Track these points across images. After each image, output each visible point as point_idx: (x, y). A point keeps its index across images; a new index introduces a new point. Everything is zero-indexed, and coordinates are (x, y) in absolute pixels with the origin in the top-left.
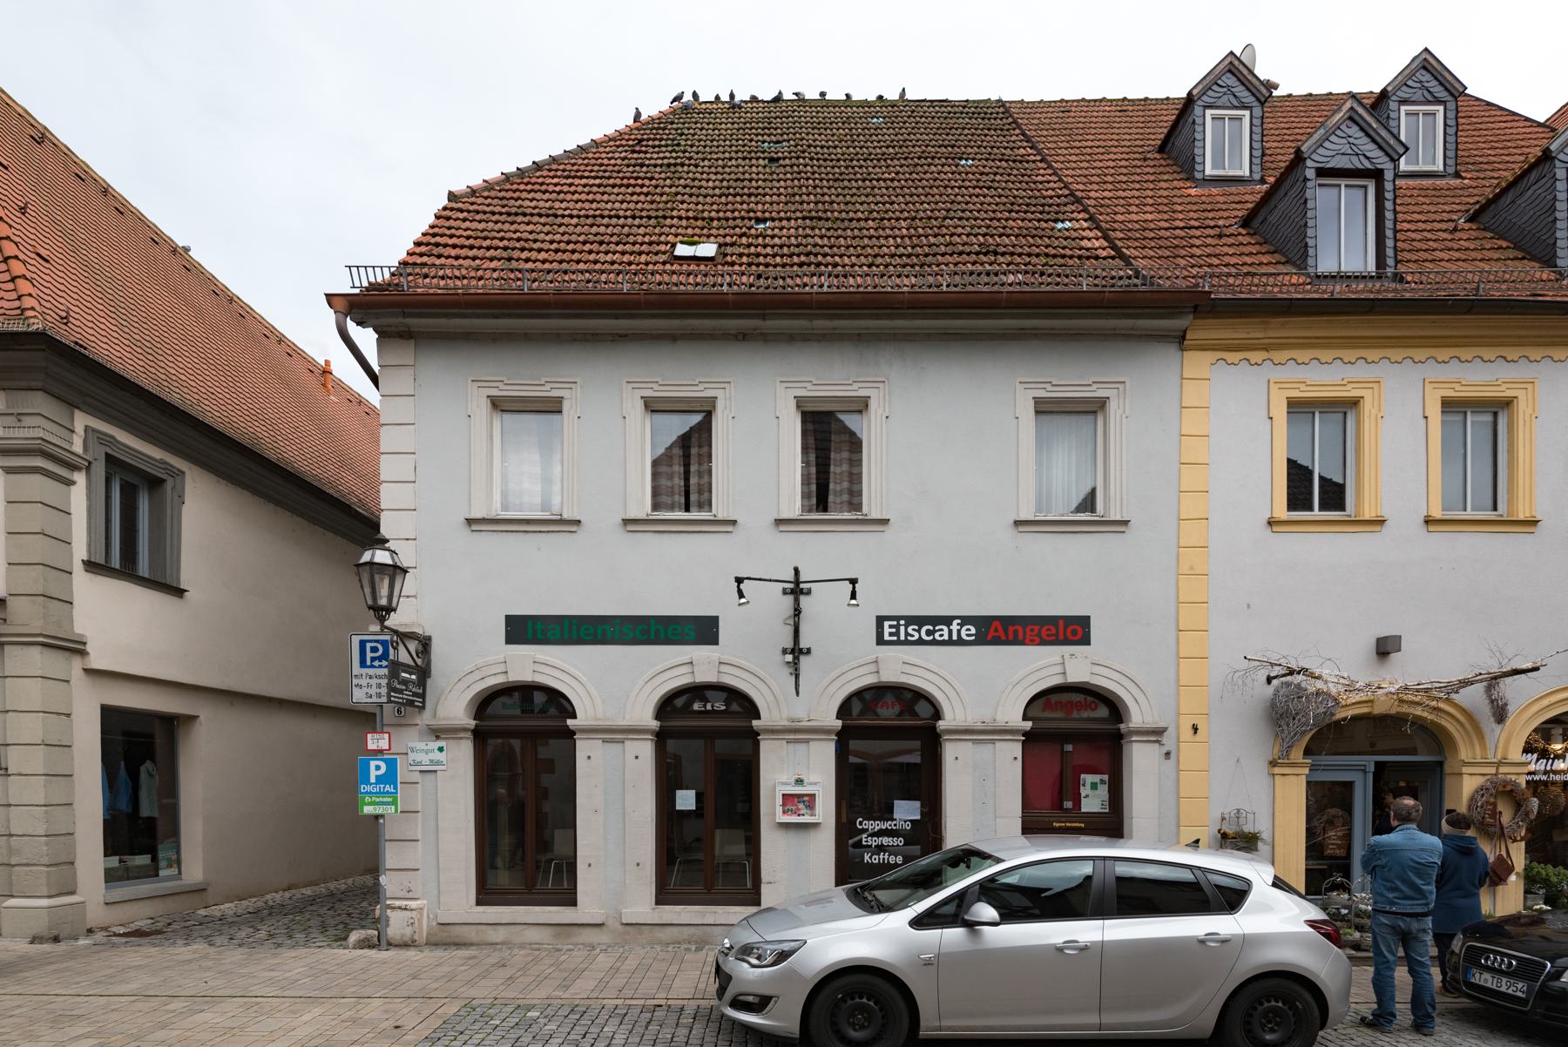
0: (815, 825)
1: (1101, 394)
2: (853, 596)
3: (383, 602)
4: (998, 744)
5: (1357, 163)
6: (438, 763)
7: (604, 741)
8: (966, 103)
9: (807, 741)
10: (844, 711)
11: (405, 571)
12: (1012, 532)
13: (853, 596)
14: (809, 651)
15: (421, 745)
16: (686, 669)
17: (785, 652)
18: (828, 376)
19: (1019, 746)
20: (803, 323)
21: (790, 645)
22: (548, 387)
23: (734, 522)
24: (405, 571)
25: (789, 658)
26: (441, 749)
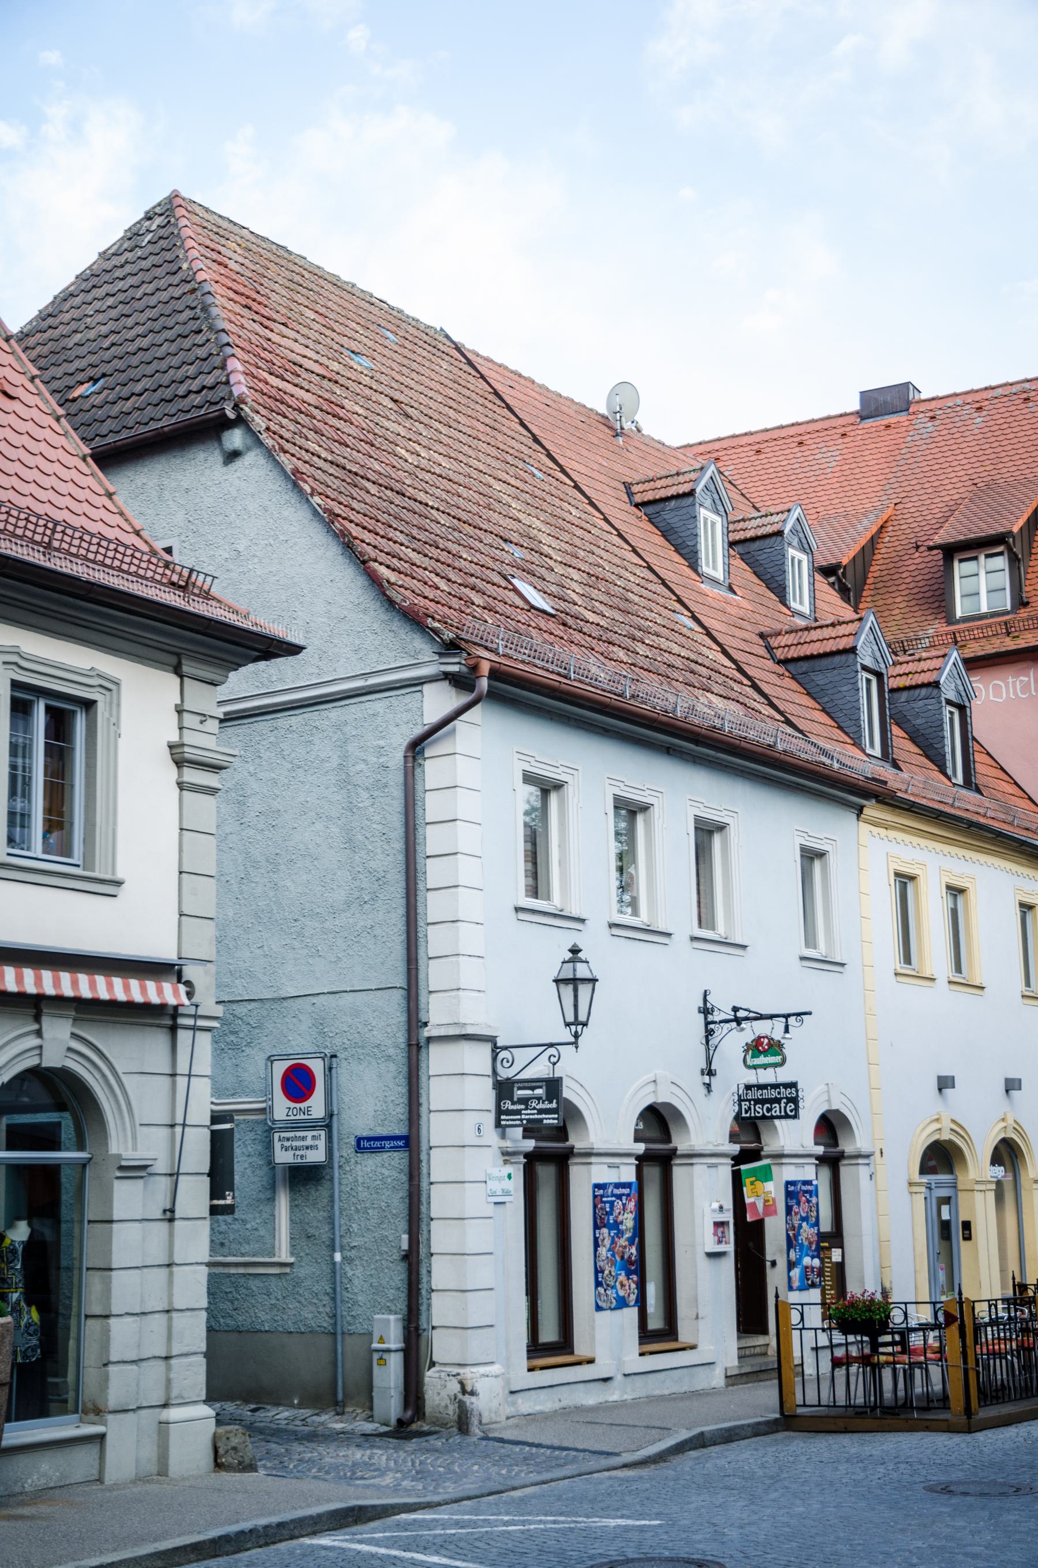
4: (806, 1167)
17: (703, 1073)
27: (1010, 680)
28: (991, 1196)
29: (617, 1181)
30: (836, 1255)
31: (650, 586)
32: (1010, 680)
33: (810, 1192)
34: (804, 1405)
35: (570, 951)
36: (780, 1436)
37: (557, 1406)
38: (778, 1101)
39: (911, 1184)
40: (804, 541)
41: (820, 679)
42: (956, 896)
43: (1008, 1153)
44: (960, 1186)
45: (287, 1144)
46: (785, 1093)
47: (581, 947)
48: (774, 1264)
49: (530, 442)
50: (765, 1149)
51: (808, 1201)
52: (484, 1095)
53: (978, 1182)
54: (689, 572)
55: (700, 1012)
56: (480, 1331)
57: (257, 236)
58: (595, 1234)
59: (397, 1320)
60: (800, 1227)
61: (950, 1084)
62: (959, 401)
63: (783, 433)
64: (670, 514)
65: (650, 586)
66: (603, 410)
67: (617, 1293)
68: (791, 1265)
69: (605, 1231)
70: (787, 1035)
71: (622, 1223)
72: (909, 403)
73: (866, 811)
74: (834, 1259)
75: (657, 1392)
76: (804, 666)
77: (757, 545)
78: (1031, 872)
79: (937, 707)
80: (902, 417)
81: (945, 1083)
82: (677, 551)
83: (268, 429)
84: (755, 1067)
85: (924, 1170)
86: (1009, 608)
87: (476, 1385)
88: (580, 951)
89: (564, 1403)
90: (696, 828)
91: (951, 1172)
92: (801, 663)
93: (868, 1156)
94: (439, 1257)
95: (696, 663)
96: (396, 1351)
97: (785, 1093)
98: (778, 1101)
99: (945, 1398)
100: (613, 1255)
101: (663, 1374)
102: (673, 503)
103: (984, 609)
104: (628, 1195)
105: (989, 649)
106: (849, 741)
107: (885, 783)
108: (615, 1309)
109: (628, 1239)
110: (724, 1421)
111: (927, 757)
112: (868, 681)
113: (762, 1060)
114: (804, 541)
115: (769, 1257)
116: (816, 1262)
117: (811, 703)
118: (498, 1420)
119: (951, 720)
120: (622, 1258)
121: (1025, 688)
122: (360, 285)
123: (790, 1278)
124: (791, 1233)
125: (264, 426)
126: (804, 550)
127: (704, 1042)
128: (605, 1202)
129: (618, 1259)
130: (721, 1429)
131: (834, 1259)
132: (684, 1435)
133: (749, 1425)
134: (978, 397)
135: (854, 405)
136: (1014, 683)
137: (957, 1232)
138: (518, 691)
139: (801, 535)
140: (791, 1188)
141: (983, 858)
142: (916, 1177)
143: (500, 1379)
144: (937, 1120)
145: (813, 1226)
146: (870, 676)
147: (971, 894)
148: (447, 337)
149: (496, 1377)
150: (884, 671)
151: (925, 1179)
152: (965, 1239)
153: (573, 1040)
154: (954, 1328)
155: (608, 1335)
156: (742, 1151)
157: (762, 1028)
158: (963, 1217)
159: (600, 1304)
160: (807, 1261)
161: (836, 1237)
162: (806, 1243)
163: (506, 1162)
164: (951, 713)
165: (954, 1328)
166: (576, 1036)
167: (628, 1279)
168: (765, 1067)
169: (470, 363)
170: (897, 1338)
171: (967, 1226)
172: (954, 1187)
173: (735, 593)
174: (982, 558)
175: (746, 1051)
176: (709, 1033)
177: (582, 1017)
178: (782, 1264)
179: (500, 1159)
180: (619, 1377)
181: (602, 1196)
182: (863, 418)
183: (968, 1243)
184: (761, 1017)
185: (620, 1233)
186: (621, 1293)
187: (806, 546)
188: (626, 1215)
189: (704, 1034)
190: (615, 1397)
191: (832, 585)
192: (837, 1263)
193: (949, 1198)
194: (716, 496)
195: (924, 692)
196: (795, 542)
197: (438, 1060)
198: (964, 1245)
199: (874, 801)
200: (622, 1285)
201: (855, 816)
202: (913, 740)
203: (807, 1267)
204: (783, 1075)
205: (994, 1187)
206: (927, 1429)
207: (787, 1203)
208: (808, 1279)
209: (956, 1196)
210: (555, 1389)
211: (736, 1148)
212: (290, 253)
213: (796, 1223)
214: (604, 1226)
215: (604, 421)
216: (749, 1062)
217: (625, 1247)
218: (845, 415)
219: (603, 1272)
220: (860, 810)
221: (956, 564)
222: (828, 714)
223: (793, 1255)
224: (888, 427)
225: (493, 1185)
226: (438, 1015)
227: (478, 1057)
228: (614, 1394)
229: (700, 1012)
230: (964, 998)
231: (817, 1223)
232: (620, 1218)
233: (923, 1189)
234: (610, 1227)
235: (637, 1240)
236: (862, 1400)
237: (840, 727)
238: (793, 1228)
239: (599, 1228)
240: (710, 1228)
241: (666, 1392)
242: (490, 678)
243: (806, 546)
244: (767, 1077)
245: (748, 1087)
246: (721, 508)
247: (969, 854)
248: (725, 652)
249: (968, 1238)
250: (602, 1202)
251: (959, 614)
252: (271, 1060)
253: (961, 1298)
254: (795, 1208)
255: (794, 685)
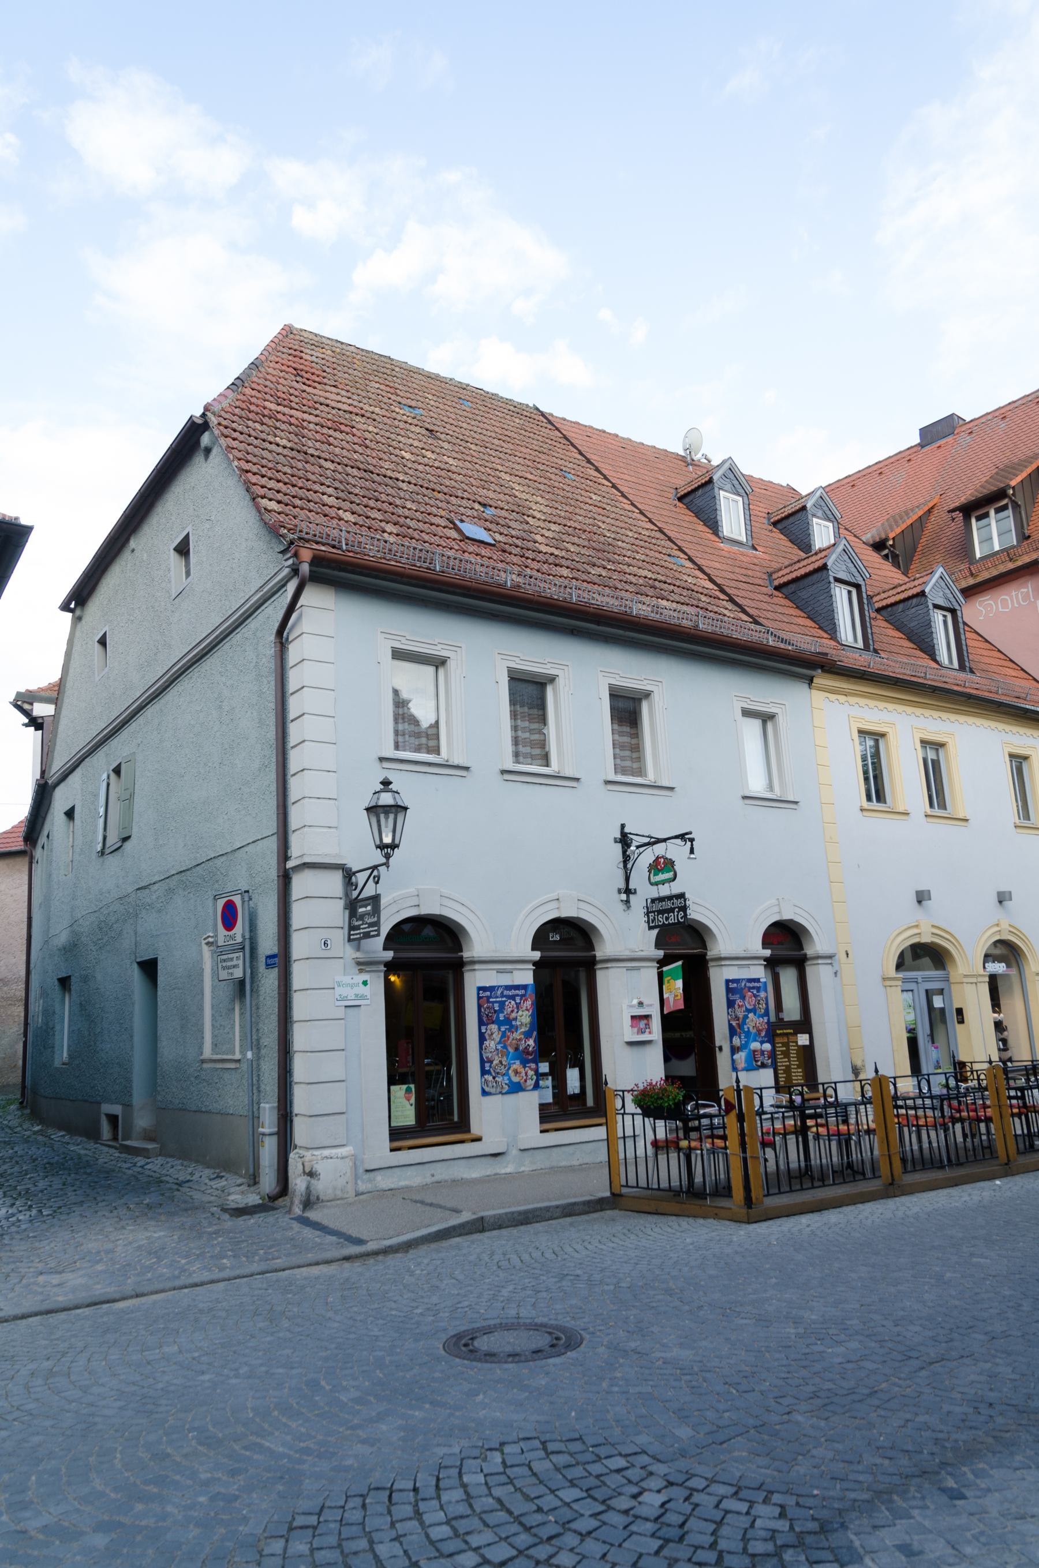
0: (649, 1042)
1: (773, 710)
2: (692, 851)
3: (387, 839)
4: (752, 967)
5: (853, 580)
6: (363, 997)
7: (628, 969)
8: (508, 402)
9: (638, 968)
10: (539, 940)
11: (406, 809)
12: (741, 802)
13: (692, 851)
14: (635, 893)
15: (347, 979)
16: (554, 905)
17: (619, 891)
18: (631, 669)
19: (531, 973)
20: (621, 632)
21: (623, 886)
22: (439, 647)
23: (577, 780)
24: (406, 809)
25: (624, 897)
26: (365, 983)
27: (1014, 593)
28: (985, 989)
29: (510, 983)
30: (803, 1039)
31: (658, 542)
32: (1014, 593)
33: (758, 989)
34: (627, 1186)
35: (382, 783)
36: (609, 1213)
37: (429, 1180)
38: (672, 910)
39: (884, 979)
40: (828, 512)
41: (804, 594)
42: (937, 750)
43: (1007, 951)
44: (952, 980)
45: (224, 964)
46: (678, 903)
47: (391, 780)
48: (721, 1048)
49: (584, 464)
50: (709, 953)
51: (755, 996)
52: (336, 913)
53: (966, 976)
54: (714, 538)
55: (616, 842)
56: (325, 1118)
57: (362, 350)
58: (480, 1030)
59: (271, 1108)
60: (746, 1017)
61: (926, 897)
62: (989, 417)
63: (870, 470)
64: (699, 500)
65: (658, 542)
66: (682, 453)
67: (510, 1079)
68: (734, 1050)
69: (494, 1027)
70: (692, 856)
71: (516, 1019)
72: (954, 428)
73: (815, 680)
74: (800, 1043)
75: (563, 1164)
76: (793, 587)
77: (791, 520)
78: (1036, 733)
79: (925, 610)
80: (950, 438)
81: (922, 897)
82: (705, 524)
83: (219, 424)
84: (657, 884)
85: (900, 966)
86: (1015, 543)
87: (315, 1166)
88: (391, 783)
89: (437, 1178)
90: (610, 695)
91: (944, 969)
92: (791, 586)
93: (830, 957)
94: (301, 1054)
95: (665, 583)
96: (270, 1134)
97: (678, 903)
98: (672, 910)
99: (729, 1188)
100: (505, 1047)
101: (572, 1147)
102: (700, 491)
103: (997, 548)
104: (522, 996)
105: (995, 573)
106: (826, 635)
107: (827, 654)
108: (507, 1093)
109: (524, 1033)
110: (549, 1200)
111: (921, 650)
112: (849, 592)
113: (662, 877)
114: (828, 512)
115: (717, 1044)
116: (767, 1046)
117: (798, 612)
118: (345, 1196)
119: (945, 622)
120: (517, 1049)
121: (1026, 597)
122: (442, 375)
123: (733, 1061)
124: (734, 1023)
125: (216, 422)
126: (829, 520)
127: (621, 865)
128: (493, 1003)
129: (511, 1050)
130: (513, 1213)
131: (800, 1043)
132: (466, 1217)
133: (557, 1207)
134: (1003, 411)
135: (917, 440)
136: (1017, 595)
137: (952, 1017)
138: (336, 573)
139: (826, 508)
140: (731, 985)
141: (971, 720)
142: (892, 972)
143: (347, 1160)
144: (917, 926)
145: (762, 1016)
146: (850, 588)
147: (951, 747)
148: (537, 409)
149: (342, 1158)
150: (862, 583)
151: (901, 975)
152: (959, 1022)
153: (384, 860)
154: (733, 1114)
155: (506, 1117)
156: (665, 955)
157: (659, 849)
158: (956, 1005)
159: (487, 1089)
160: (755, 1045)
161: (805, 1024)
162: (753, 1031)
163: (361, 971)
164: (945, 616)
165: (733, 1114)
166: (388, 857)
167: (525, 1067)
168: (663, 882)
169: (550, 422)
170: (1019, 1094)
171: (960, 1012)
172: (947, 980)
173: (756, 550)
174: (992, 512)
175: (650, 871)
176: (626, 858)
177: (397, 842)
178: (727, 1049)
179: (356, 970)
180: (514, 1152)
181: (488, 998)
182: (923, 447)
183: (961, 1026)
184: (659, 841)
185: (513, 1028)
186: (516, 1079)
187: (831, 516)
188: (520, 1013)
189: (621, 859)
190: (508, 1170)
191: (886, 557)
192: (804, 1046)
193: (943, 990)
194: (735, 482)
195: (914, 601)
196: (820, 513)
197: (301, 884)
198: (959, 1027)
199: (820, 671)
200: (516, 1072)
201: (806, 686)
202: (910, 639)
203: (754, 1051)
204: (675, 888)
205: (987, 979)
206: (716, 1216)
207: (728, 999)
208: (757, 1061)
209: (950, 988)
210: (427, 1166)
211: (660, 953)
212: (392, 360)
213: (741, 1015)
214: (493, 1023)
215: (683, 459)
216: (652, 880)
217: (520, 1040)
218: (912, 447)
219: (491, 1062)
220: (810, 680)
221: (973, 521)
222: (811, 619)
223: (736, 1041)
224: (939, 447)
225: (339, 991)
226: (300, 849)
227: (334, 883)
228: (507, 1167)
229: (616, 842)
230: (942, 829)
231: (767, 1013)
232: (514, 1015)
233: (900, 983)
234: (500, 1024)
235: (535, 1033)
236: (797, 1165)
237: (821, 628)
238: (737, 1018)
239: (487, 1025)
240: (628, 1021)
241: (576, 1163)
242: (311, 564)
243: (831, 516)
244: (665, 891)
245: (653, 901)
246: (741, 491)
247: (944, 715)
248: (711, 580)
249: (961, 1021)
250: (488, 1002)
251: (978, 555)
252: (215, 898)
253: (738, 1086)
254: (739, 1002)
255: (787, 603)
